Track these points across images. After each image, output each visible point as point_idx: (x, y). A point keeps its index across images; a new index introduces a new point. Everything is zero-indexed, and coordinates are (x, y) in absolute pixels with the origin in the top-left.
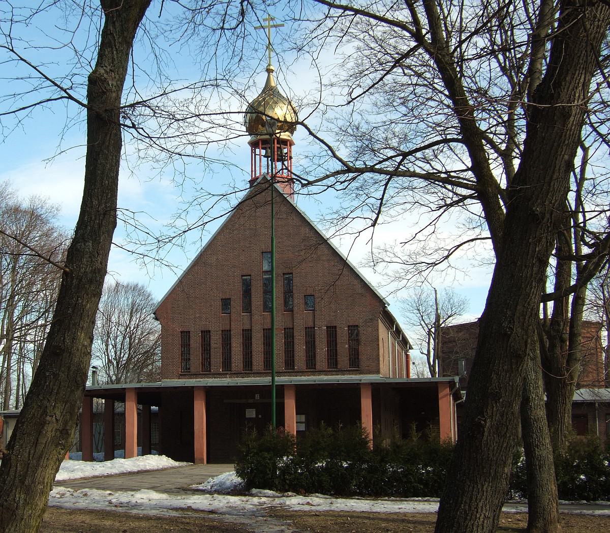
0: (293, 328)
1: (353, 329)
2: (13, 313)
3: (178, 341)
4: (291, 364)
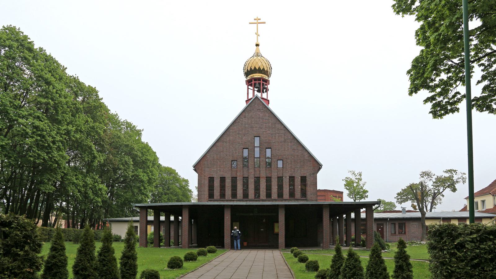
0: (271, 177)
1: (303, 179)
2: (19, 273)
3: (207, 182)
4: (212, 187)
